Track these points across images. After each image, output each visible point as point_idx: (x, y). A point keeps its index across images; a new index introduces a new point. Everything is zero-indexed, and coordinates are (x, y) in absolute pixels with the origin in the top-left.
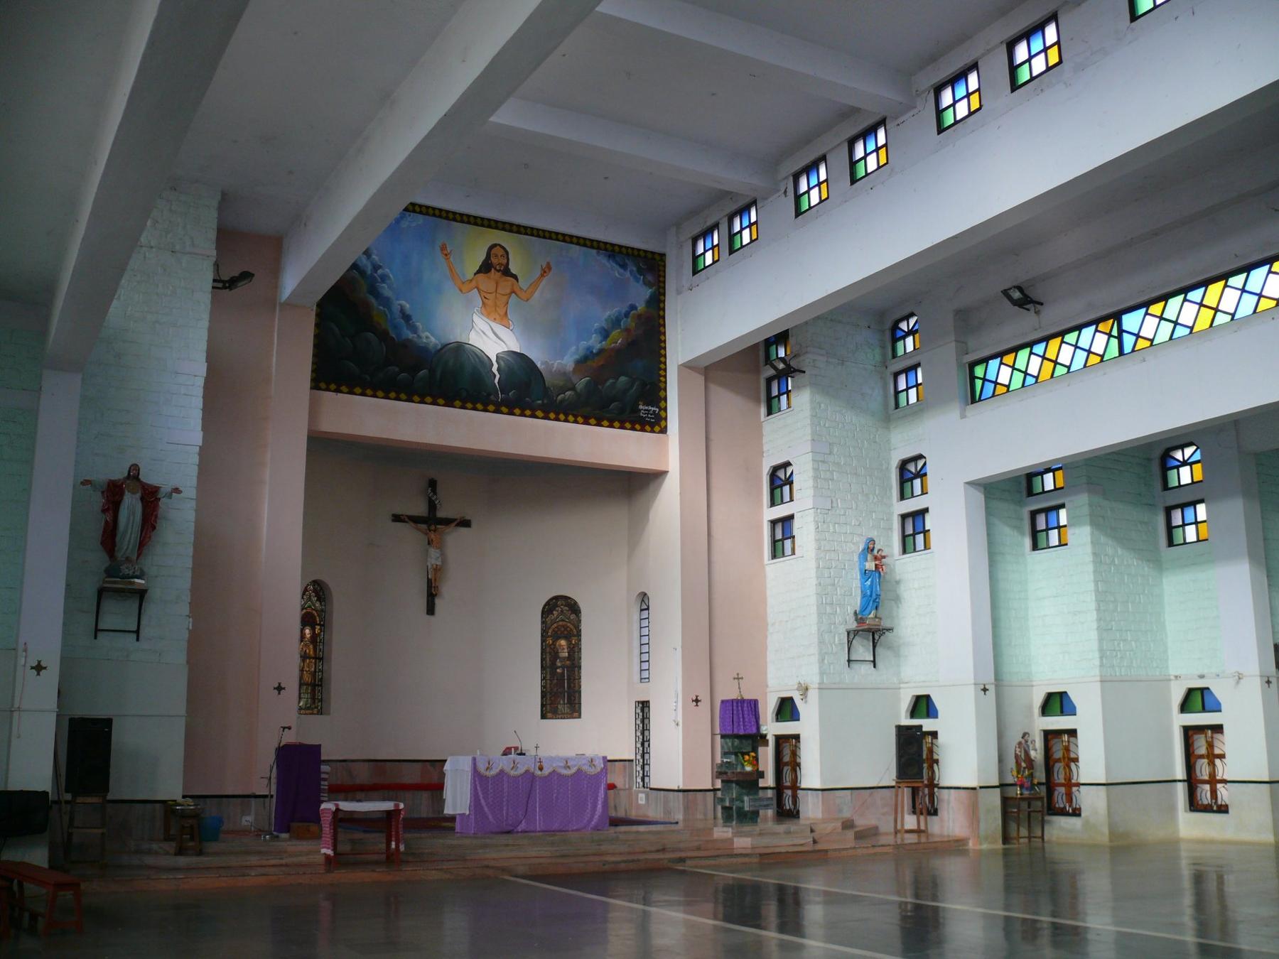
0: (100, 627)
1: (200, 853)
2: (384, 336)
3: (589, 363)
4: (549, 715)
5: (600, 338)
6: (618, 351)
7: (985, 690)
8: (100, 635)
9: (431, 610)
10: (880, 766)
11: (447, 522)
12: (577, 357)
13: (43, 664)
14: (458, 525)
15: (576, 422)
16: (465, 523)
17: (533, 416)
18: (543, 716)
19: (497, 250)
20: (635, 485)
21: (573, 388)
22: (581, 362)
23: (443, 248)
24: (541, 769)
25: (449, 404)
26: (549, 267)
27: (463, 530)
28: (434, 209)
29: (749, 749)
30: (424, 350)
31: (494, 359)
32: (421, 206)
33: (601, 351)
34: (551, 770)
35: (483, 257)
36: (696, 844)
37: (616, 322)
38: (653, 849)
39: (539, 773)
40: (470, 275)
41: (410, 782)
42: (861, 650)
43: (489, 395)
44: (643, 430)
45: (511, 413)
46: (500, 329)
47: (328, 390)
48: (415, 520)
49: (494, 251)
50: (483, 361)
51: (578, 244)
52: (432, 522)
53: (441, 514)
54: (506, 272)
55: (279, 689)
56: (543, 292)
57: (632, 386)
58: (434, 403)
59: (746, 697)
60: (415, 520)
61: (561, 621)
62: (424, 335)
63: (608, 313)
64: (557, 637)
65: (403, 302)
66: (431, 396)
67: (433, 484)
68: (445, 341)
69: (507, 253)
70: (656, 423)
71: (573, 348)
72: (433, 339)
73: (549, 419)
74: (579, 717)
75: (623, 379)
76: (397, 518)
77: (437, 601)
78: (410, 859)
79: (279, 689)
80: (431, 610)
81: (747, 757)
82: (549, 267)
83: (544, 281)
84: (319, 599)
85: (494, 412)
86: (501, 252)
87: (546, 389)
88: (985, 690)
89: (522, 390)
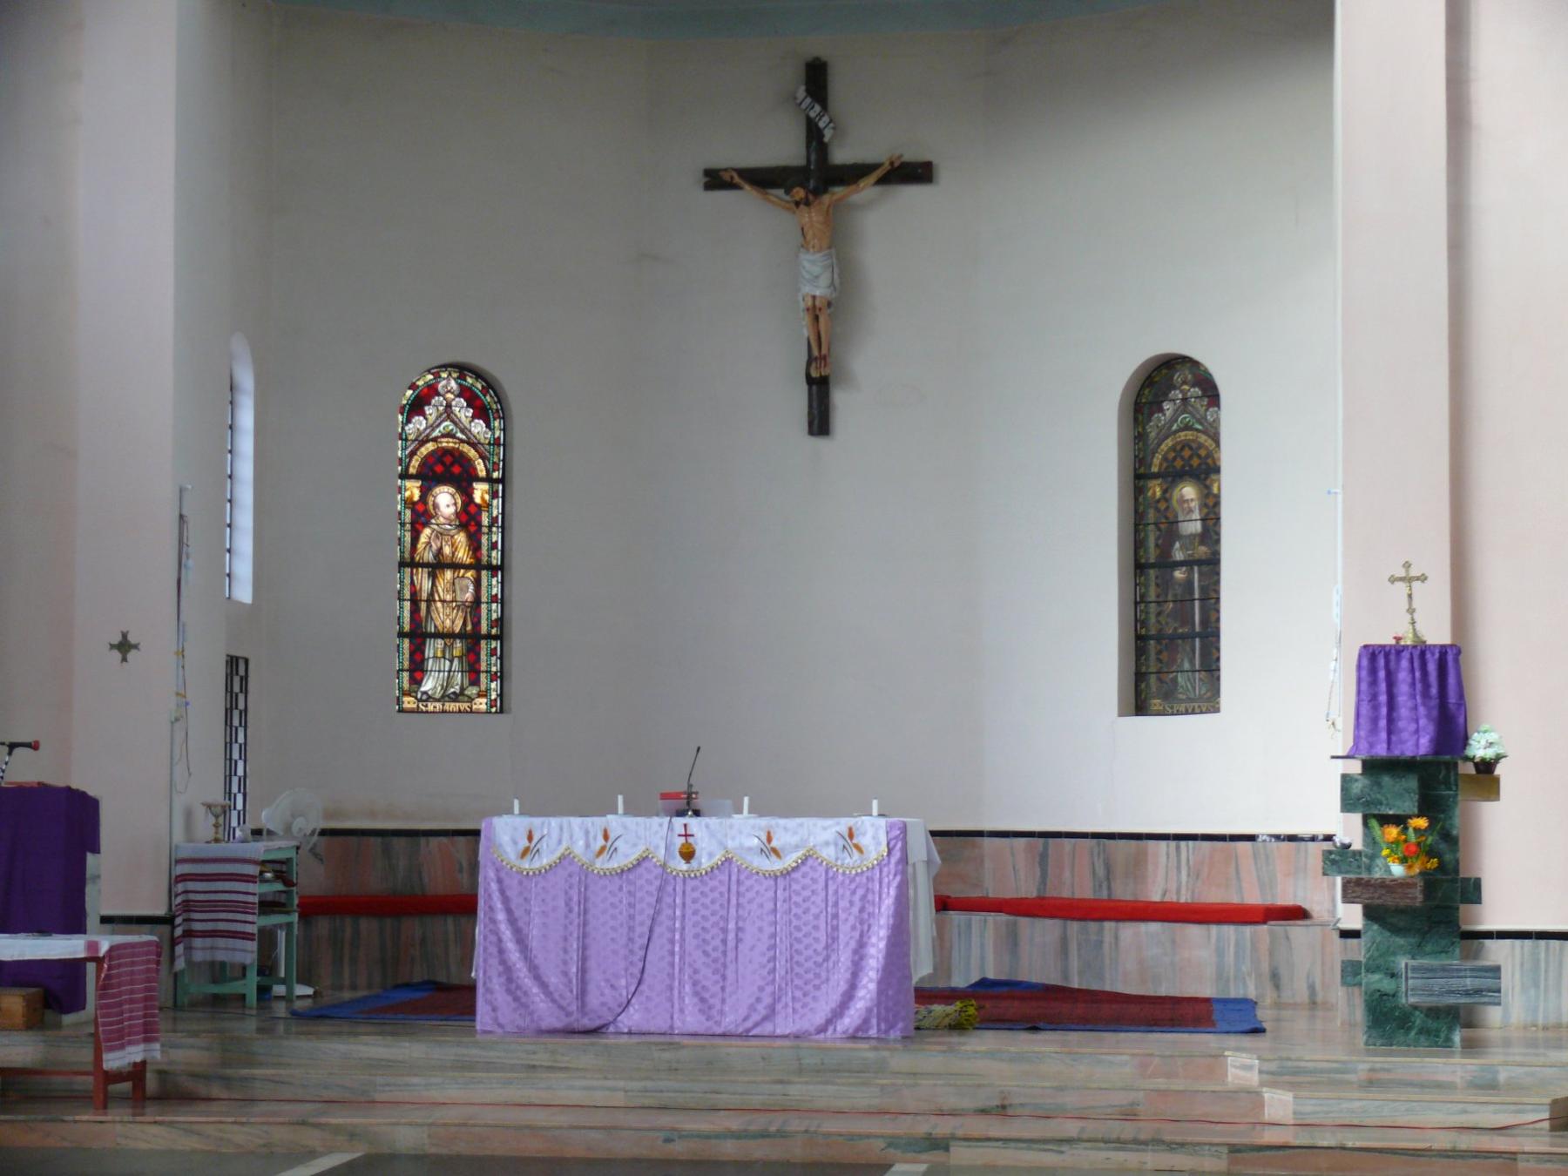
4: (1156, 703)
9: (820, 423)
11: (854, 174)
13: (117, 639)
14: (884, 180)
16: (917, 173)
18: (1140, 706)
24: (688, 854)
29: (1408, 805)
34: (718, 857)
36: (1121, 1099)
38: (967, 1103)
39: (683, 866)
48: (763, 179)
52: (816, 179)
53: (842, 155)
55: (124, 646)
60: (763, 179)
61: (1170, 424)
64: (1173, 476)
67: (816, 77)
74: (1209, 701)
76: (715, 180)
77: (840, 399)
78: (216, 1091)
79: (124, 646)
80: (820, 423)
81: (1393, 832)
84: (481, 412)
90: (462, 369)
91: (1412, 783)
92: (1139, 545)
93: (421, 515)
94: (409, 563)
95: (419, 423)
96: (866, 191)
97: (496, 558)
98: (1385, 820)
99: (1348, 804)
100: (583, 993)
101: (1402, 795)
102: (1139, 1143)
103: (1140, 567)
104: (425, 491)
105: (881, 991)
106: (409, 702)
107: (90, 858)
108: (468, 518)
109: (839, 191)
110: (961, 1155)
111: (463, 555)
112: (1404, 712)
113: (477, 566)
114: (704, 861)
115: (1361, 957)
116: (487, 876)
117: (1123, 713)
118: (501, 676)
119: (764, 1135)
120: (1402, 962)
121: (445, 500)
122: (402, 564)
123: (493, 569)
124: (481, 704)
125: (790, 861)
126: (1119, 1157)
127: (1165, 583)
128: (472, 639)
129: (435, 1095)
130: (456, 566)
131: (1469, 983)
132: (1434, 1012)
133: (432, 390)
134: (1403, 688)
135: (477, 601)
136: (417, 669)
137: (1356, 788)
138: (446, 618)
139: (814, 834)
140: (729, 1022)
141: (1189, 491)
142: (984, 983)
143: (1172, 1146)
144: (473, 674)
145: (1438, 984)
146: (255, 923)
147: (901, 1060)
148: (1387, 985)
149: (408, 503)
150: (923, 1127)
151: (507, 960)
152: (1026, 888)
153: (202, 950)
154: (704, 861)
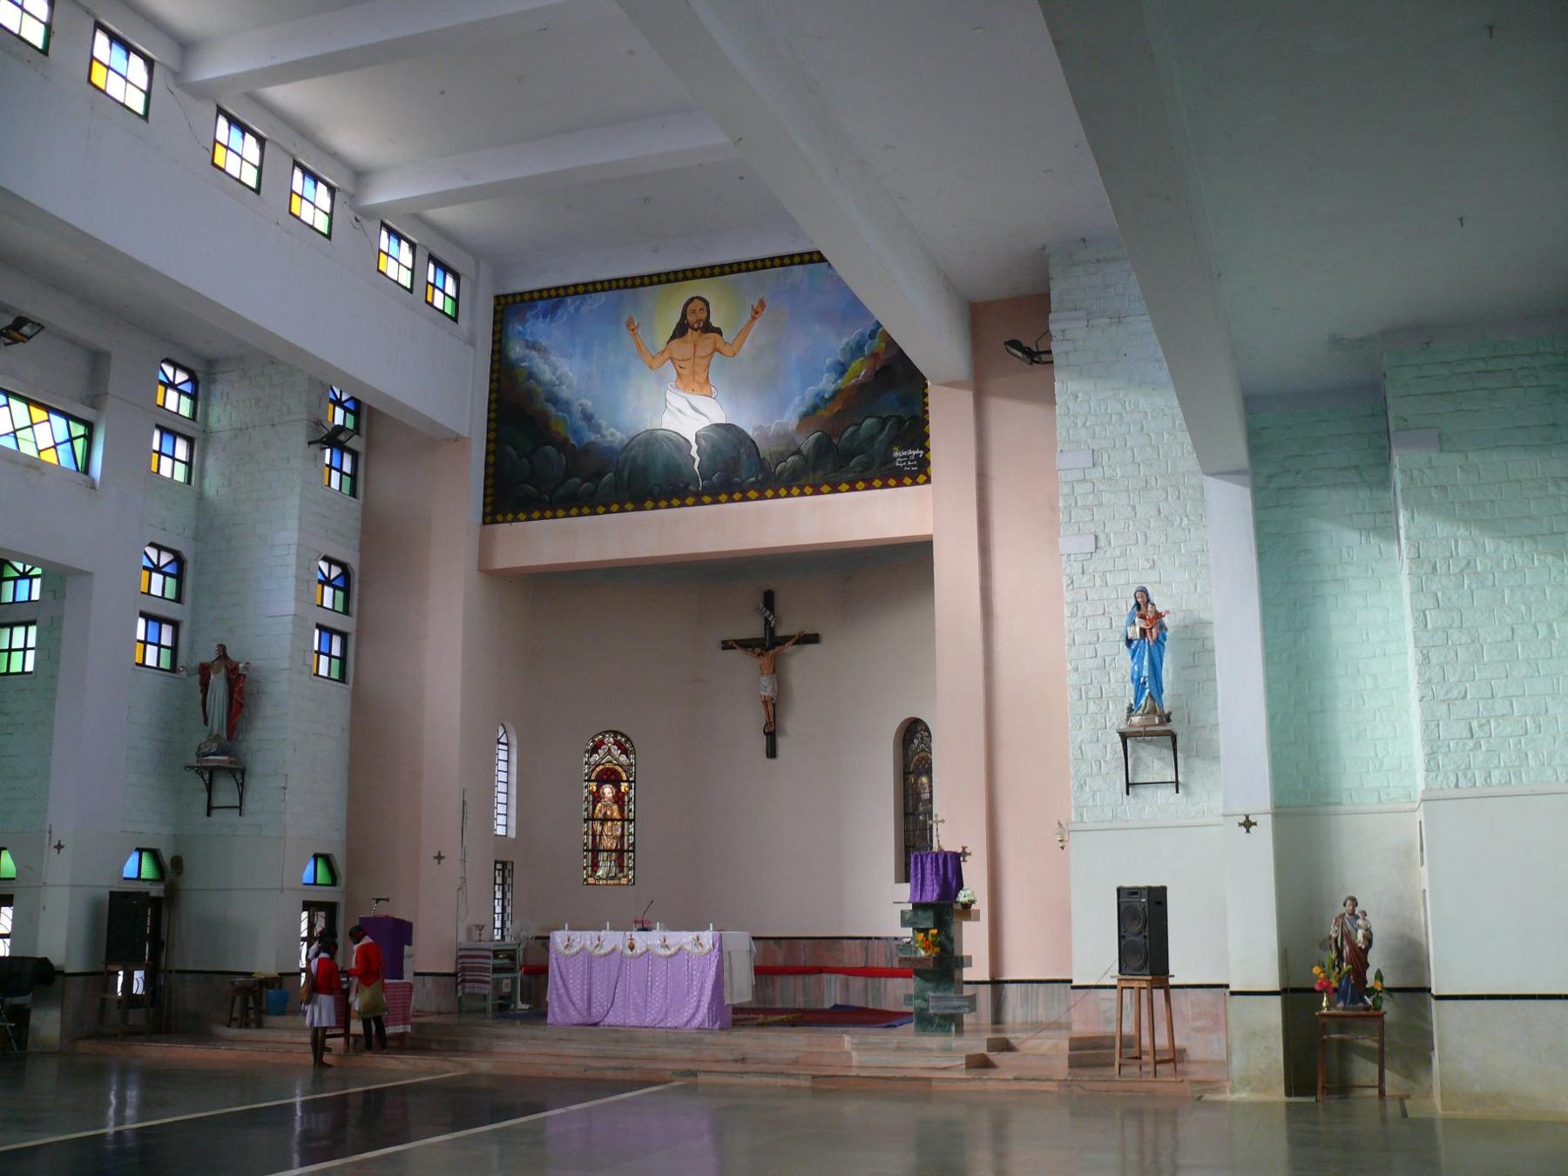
0: (215, 804)
1: (260, 1026)
2: (563, 445)
3: (819, 413)
5: (833, 376)
6: (861, 388)
7: (1248, 824)
8: (214, 812)
9: (772, 752)
10: (1095, 953)
11: (785, 640)
12: (803, 409)
13: (1252, 829)
14: (798, 642)
15: (802, 494)
16: (813, 639)
17: (745, 499)
19: (698, 305)
20: (909, 561)
21: (798, 452)
22: (807, 417)
23: (630, 323)
24: (632, 947)
25: (639, 507)
26: (762, 304)
27: (810, 648)
28: (617, 280)
29: (929, 924)
30: (610, 450)
31: (692, 440)
32: (602, 282)
33: (835, 393)
35: (677, 318)
36: (792, 1056)
37: (857, 350)
39: (629, 952)
40: (661, 345)
41: (853, 965)
42: (1157, 765)
43: (687, 485)
44: (900, 484)
45: (716, 502)
46: (701, 401)
47: (504, 521)
48: (746, 645)
49: (691, 306)
50: (681, 444)
51: (802, 262)
53: (780, 633)
54: (707, 328)
55: (439, 857)
56: (758, 335)
57: (883, 429)
58: (622, 510)
59: (946, 849)
60: (746, 645)
62: (607, 433)
63: (845, 340)
65: (584, 401)
66: (863, 480)
67: (769, 599)
68: (632, 433)
69: (707, 304)
70: (919, 472)
71: (797, 401)
72: (618, 434)
73: (749, 499)
75: (869, 422)
76: (726, 646)
77: (781, 742)
80: (772, 752)
82: (762, 304)
83: (756, 324)
84: (624, 751)
85: (757, 499)
86: (700, 304)
87: (761, 461)
88: (1248, 824)
89: (737, 470)
90: (616, 733)
91: (931, 914)
92: (906, 805)
93: (597, 797)
94: (591, 819)
95: (596, 757)
96: (789, 648)
97: (631, 815)
98: (920, 930)
99: (904, 923)
100: (589, 1008)
101: (927, 920)
102: (774, 1074)
103: (906, 815)
104: (599, 787)
105: (710, 1009)
106: (591, 880)
107: (406, 948)
108: (619, 799)
109: (778, 649)
110: (702, 1078)
111: (616, 815)
112: (928, 882)
113: (623, 820)
114: (638, 951)
115: (912, 991)
116: (552, 955)
117: (898, 881)
118: (634, 868)
119: (623, 1069)
120: (931, 994)
121: (608, 791)
122: (586, 821)
123: (630, 821)
124: (624, 881)
125: (673, 950)
126: (766, 1080)
127: (916, 821)
128: (620, 852)
129: (909, 1064)
130: (613, 820)
131: (956, 1003)
132: (943, 1017)
133: (602, 743)
134: (928, 871)
135: (622, 835)
136: (595, 866)
137: (907, 916)
138: (608, 843)
139: (685, 938)
140: (648, 1022)
141: (924, 779)
142: (836, 1006)
143: (789, 1075)
144: (621, 867)
145: (943, 1003)
146: (490, 977)
147: (723, 1038)
148: (923, 1005)
149: (591, 792)
150: (685, 1066)
151: (566, 996)
152: (859, 962)
153: (469, 988)
154: (638, 951)
